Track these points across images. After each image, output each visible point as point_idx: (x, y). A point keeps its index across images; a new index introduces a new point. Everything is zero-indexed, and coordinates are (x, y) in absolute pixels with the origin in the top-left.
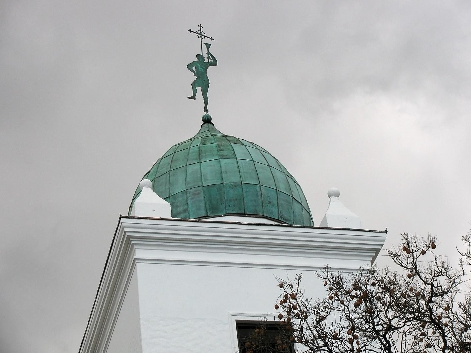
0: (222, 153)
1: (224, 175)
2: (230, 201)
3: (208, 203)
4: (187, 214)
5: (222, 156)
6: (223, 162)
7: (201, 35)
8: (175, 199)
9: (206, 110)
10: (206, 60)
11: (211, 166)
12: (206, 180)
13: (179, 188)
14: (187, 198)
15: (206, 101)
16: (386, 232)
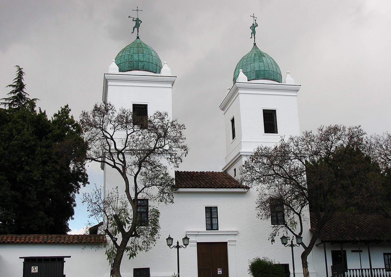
0: (260, 60)
1: (260, 67)
2: (262, 75)
3: (256, 75)
4: (251, 78)
5: (260, 61)
6: (260, 63)
7: (254, 17)
8: (248, 73)
9: (255, 41)
10: (255, 25)
11: (257, 64)
12: (256, 69)
13: (249, 70)
14: (251, 73)
15: (138, 31)
16: (301, 86)
